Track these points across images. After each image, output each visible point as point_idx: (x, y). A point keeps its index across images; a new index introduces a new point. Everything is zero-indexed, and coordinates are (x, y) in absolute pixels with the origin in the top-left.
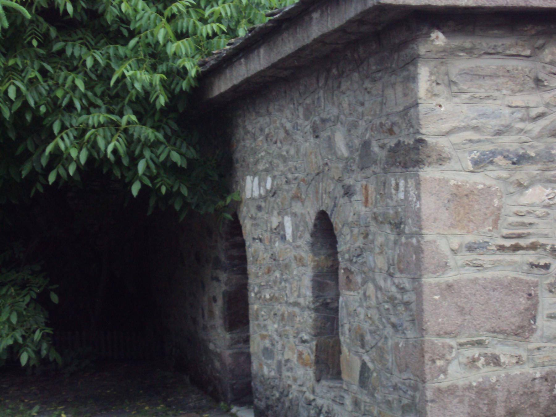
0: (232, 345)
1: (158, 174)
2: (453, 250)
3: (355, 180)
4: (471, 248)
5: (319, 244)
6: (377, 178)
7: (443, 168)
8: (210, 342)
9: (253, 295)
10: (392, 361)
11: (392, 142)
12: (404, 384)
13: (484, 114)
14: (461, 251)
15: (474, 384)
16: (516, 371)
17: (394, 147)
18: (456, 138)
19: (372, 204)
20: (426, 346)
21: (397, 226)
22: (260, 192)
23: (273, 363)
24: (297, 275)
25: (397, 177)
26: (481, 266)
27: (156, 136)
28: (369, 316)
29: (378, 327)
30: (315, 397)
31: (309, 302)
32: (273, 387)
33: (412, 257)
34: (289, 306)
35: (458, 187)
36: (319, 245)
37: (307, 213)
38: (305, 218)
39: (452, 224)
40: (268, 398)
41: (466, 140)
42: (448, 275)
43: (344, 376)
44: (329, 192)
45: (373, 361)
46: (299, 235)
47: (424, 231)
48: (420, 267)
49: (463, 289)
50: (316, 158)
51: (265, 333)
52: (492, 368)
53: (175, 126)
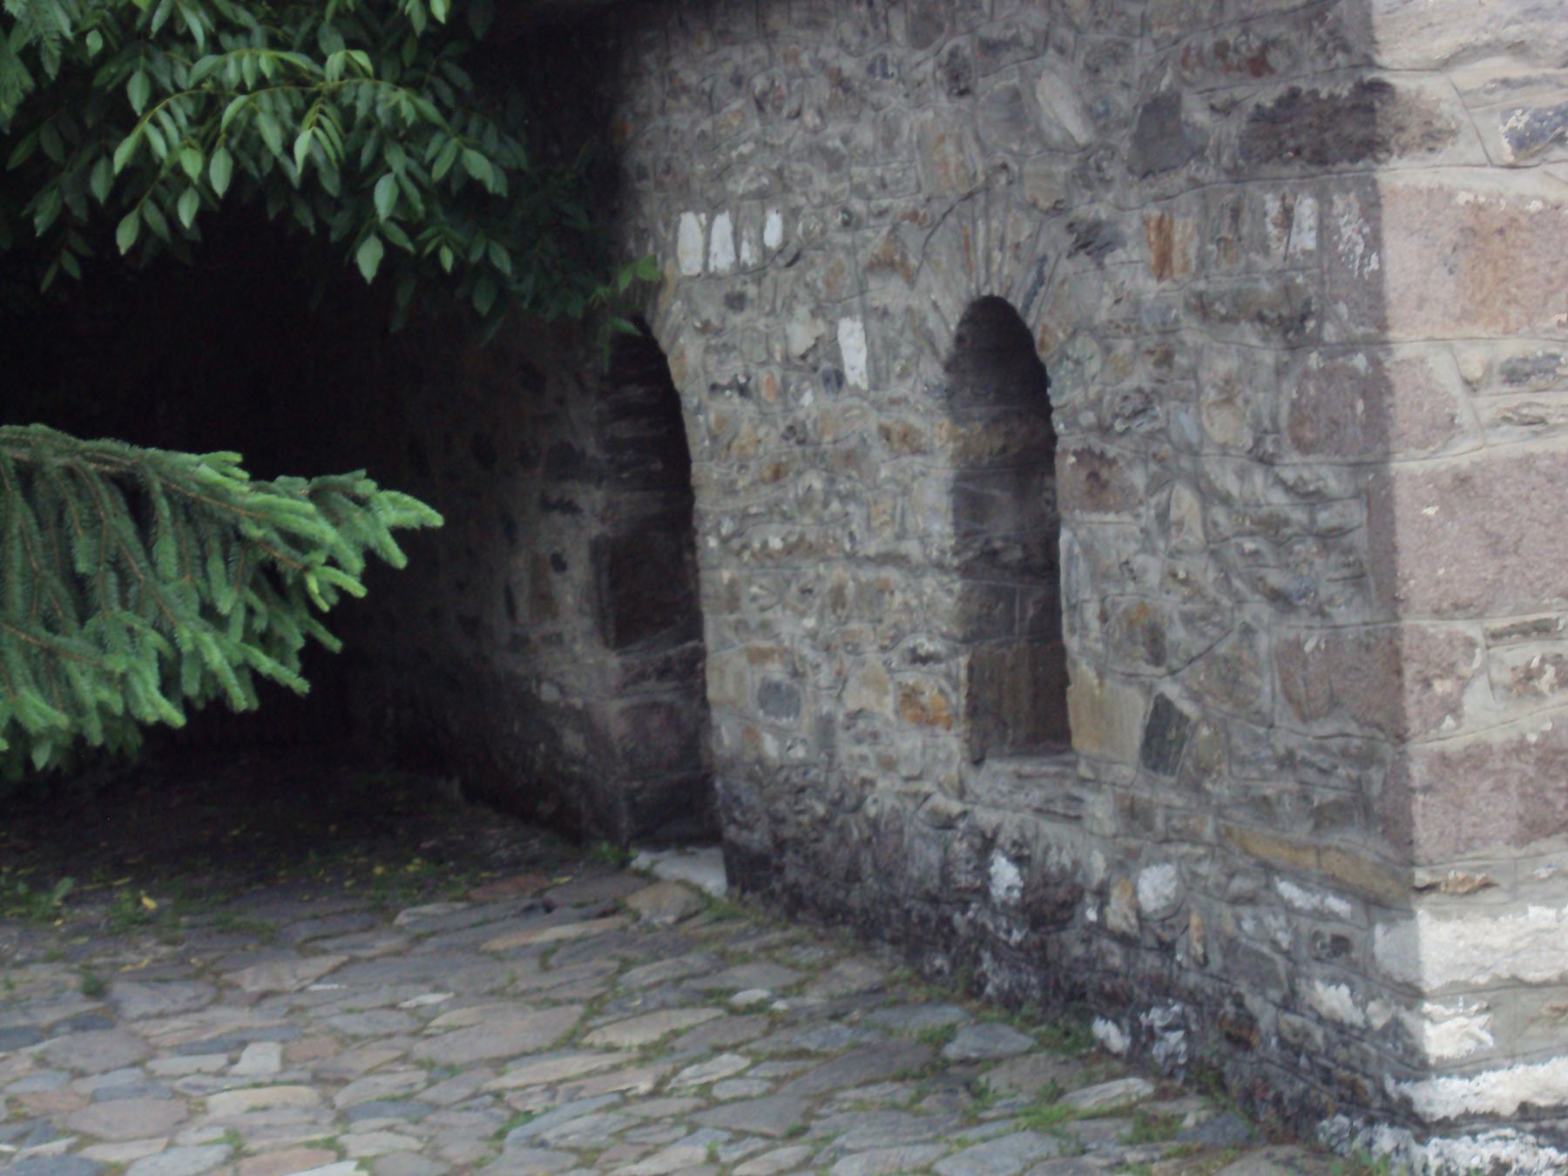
0: (625, 686)
1: (429, 214)
2: (1468, 382)
3: (1123, 206)
4: (1514, 375)
5: (968, 390)
6: (1204, 196)
7: (1438, 158)
8: (539, 682)
9: (713, 542)
10: (1273, 690)
11: (1267, 94)
12: (1322, 749)
13: (1537, 9)
14: (1489, 384)
15: (1532, 738)
17: (1272, 110)
18: (1471, 76)
19: (1185, 269)
20: (1407, 643)
21: (1292, 324)
22: (738, 256)
23: (804, 724)
24: (891, 480)
25: (1286, 189)
26: (1542, 421)
27: (419, 112)
28: (1182, 575)
29: (1216, 603)
30: (969, 807)
31: (943, 552)
32: (802, 790)
33: (1353, 407)
34: (859, 566)
35: (1478, 208)
36: (967, 391)
37: (927, 306)
38: (924, 320)
39: (1464, 311)
40: (778, 820)
41: (1494, 81)
42: (1456, 451)
43: (1082, 741)
44: (1017, 246)
45: (1196, 697)
46: (898, 369)
47: (1392, 335)
48: (1384, 432)
49: (1498, 487)
50: (961, 150)
51: (766, 644)
53: (462, 79)
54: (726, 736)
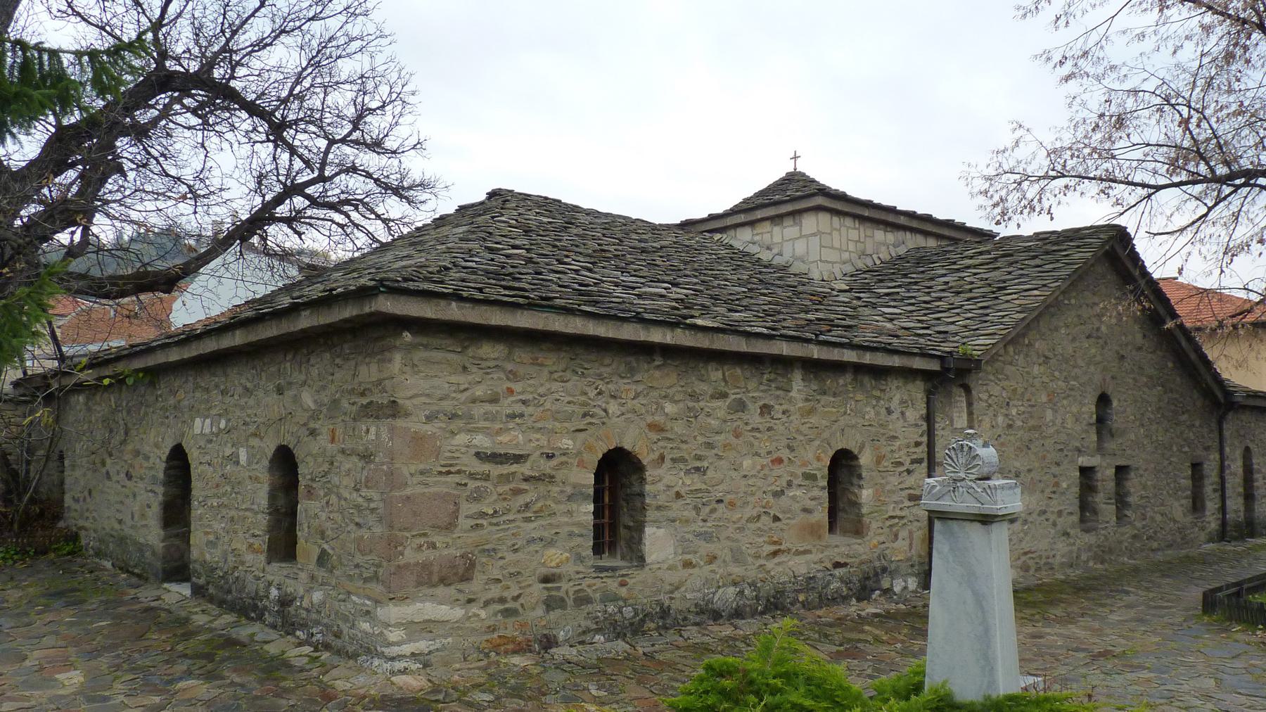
4: (422, 473)
11: (365, 401)
16: (446, 552)
18: (416, 401)
52: (431, 550)
54: (195, 554)
